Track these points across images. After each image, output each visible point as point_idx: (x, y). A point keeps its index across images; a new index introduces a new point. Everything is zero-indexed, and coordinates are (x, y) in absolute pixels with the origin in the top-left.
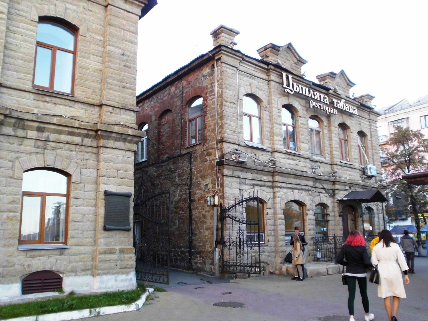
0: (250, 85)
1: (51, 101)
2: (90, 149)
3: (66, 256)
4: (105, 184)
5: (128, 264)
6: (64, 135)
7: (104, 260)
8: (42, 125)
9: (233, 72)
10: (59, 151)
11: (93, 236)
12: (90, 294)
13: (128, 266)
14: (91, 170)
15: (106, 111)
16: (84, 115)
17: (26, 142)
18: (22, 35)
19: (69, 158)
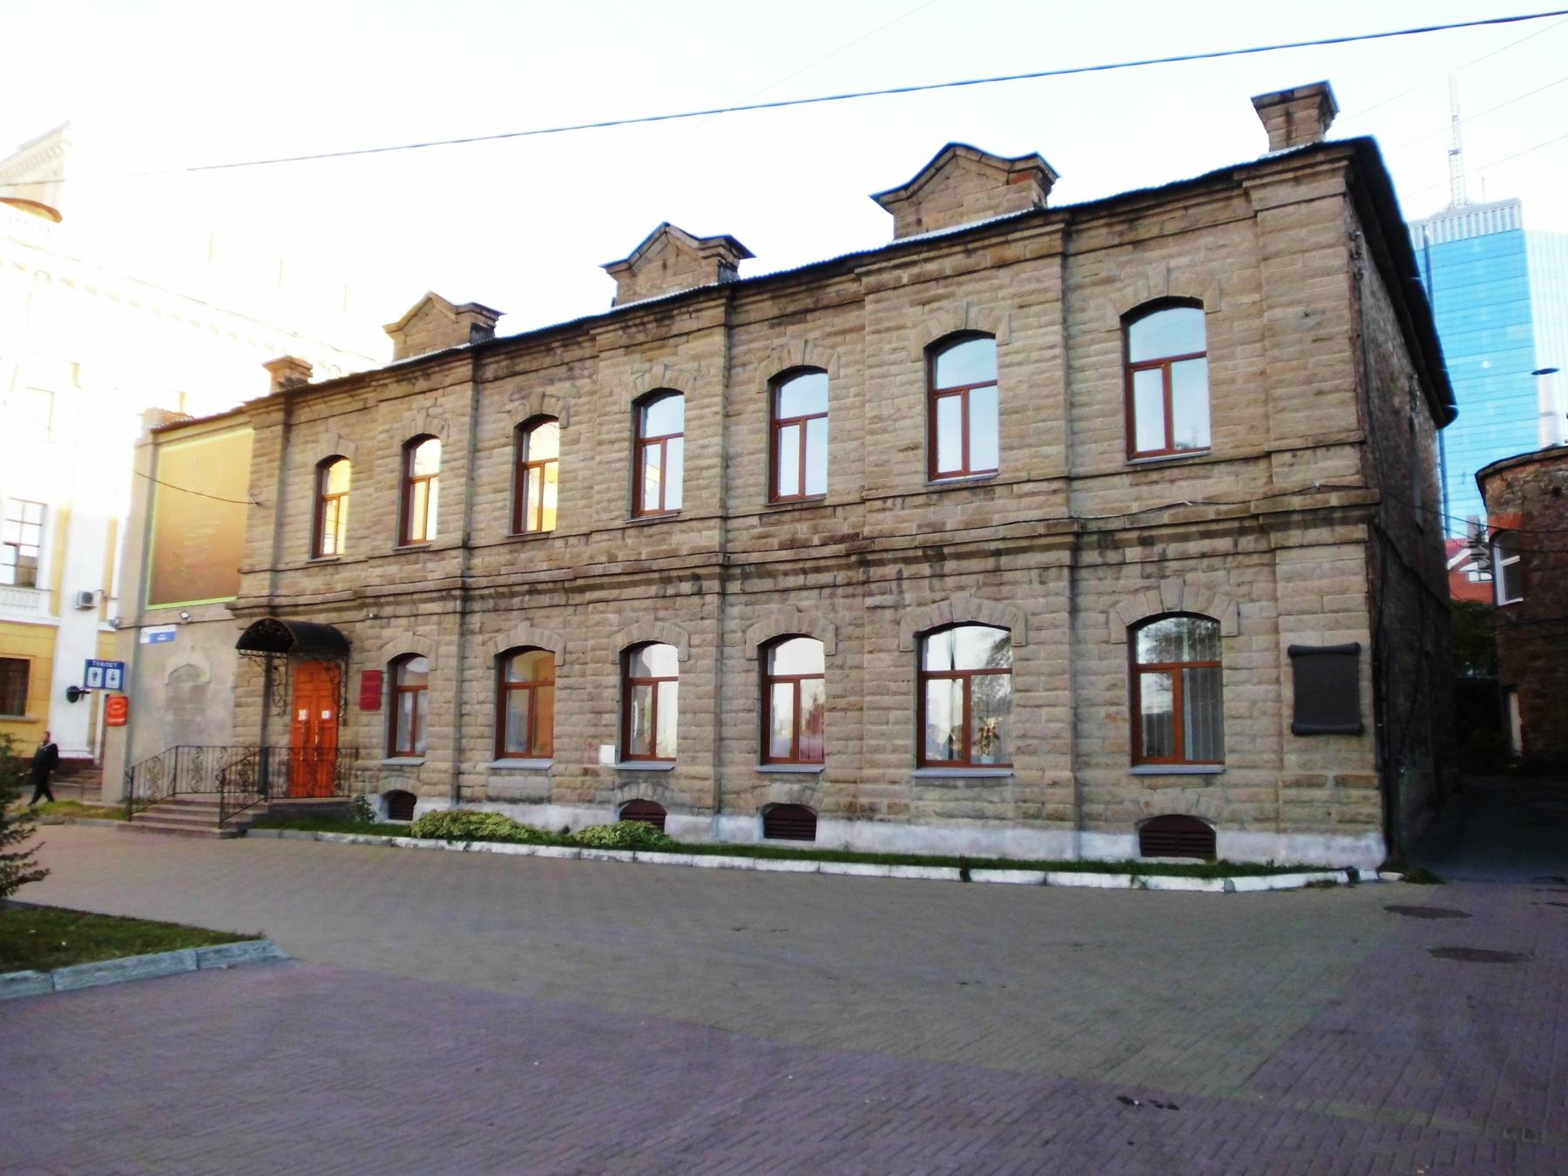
2: (1255, 559)
4: (1292, 630)
8: (1146, 533)
10: (1189, 576)
11: (1275, 747)
14: (1264, 603)
17: (1126, 570)
18: (1095, 366)
19: (1211, 587)
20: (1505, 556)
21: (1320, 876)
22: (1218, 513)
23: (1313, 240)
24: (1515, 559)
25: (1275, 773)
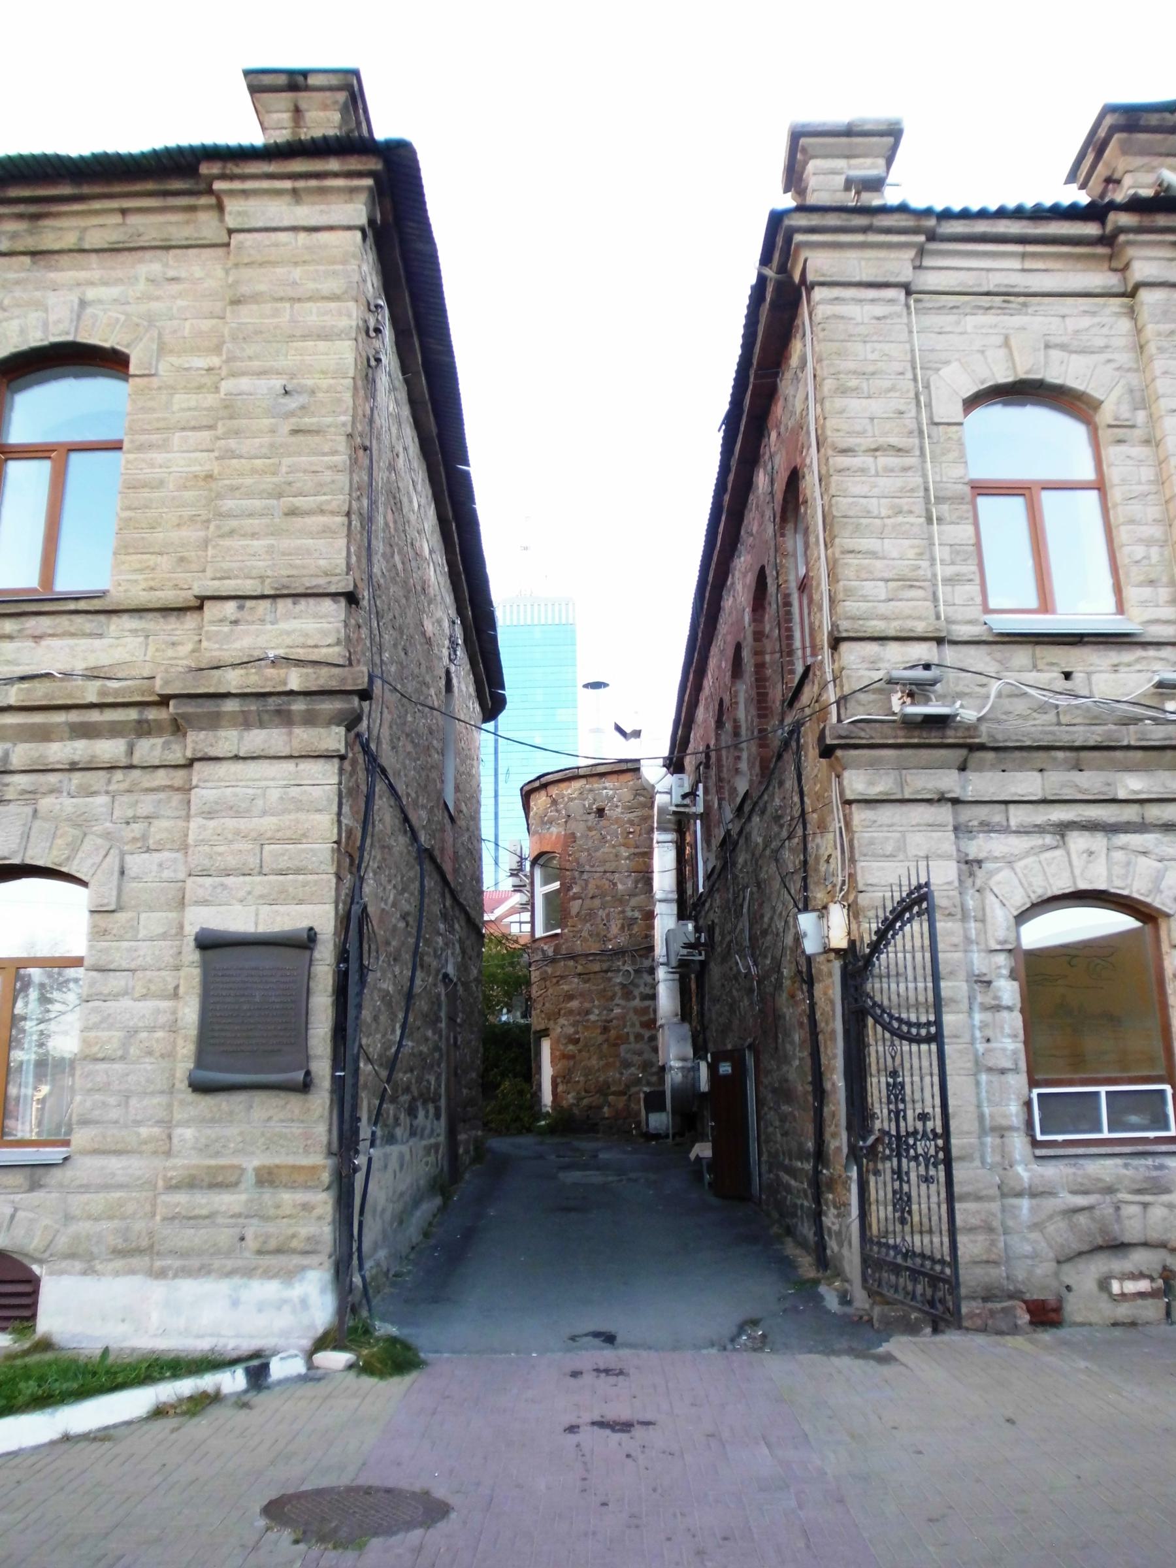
0: (1006, 343)
1: (20, 631)
3: (54, 1195)
4: (205, 903)
5: (294, 1236)
6: (62, 740)
7: (184, 1213)
9: (879, 310)
10: (46, 803)
12: (172, 1355)
13: (294, 1244)
14: (166, 855)
15: (212, 622)
16: (133, 654)
19: (82, 823)
20: (546, 881)
21: (186, 1386)
22: (102, 693)
23: (311, 285)
24: (556, 885)
25: (158, 1163)
